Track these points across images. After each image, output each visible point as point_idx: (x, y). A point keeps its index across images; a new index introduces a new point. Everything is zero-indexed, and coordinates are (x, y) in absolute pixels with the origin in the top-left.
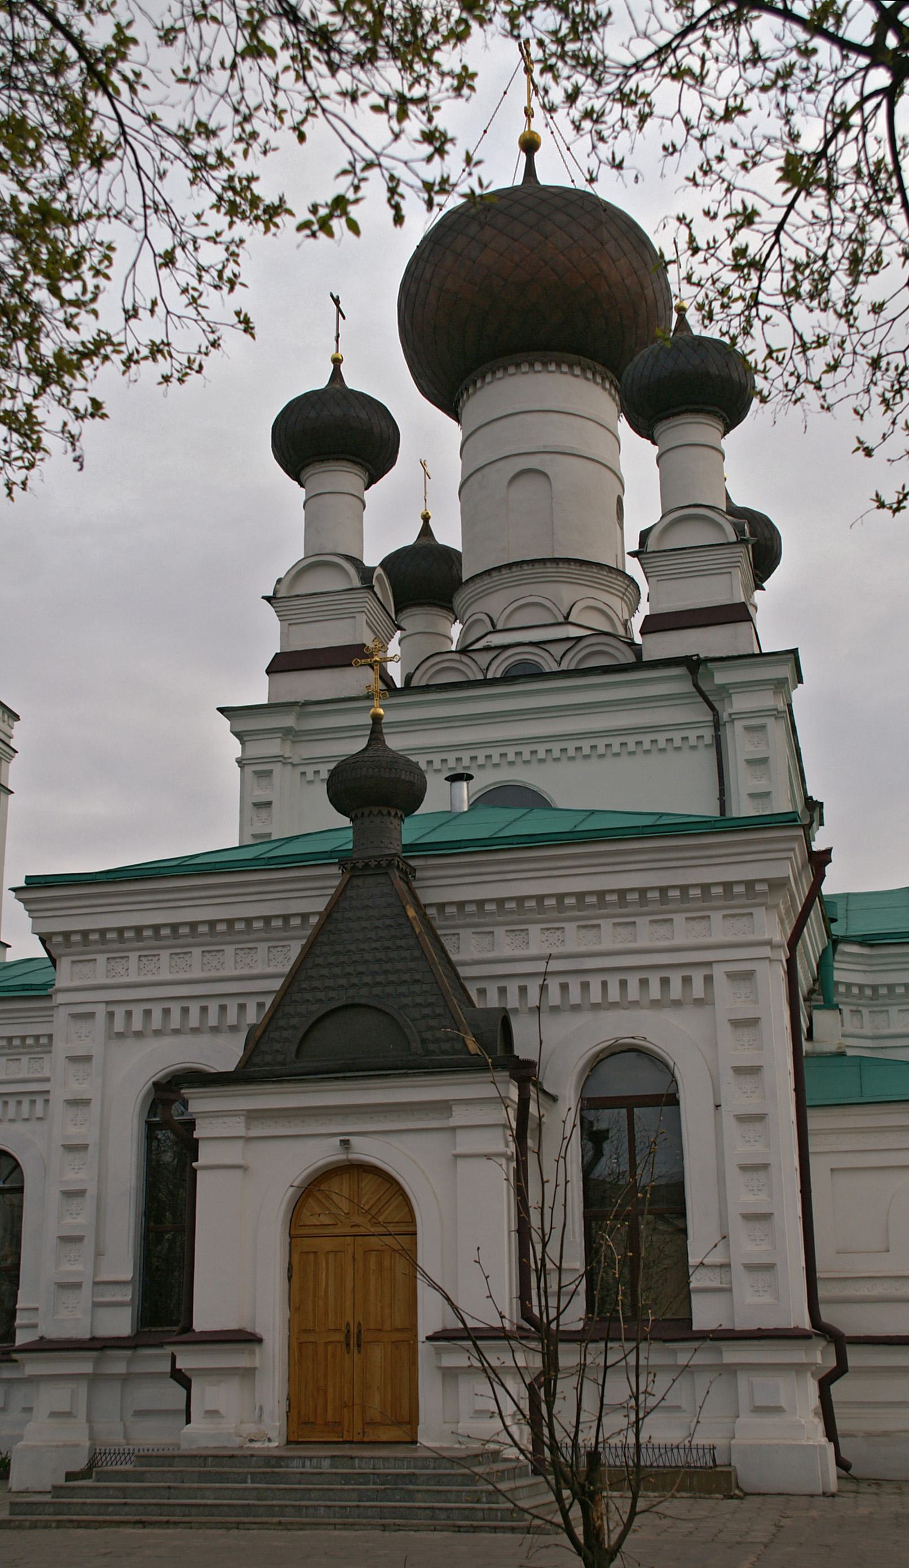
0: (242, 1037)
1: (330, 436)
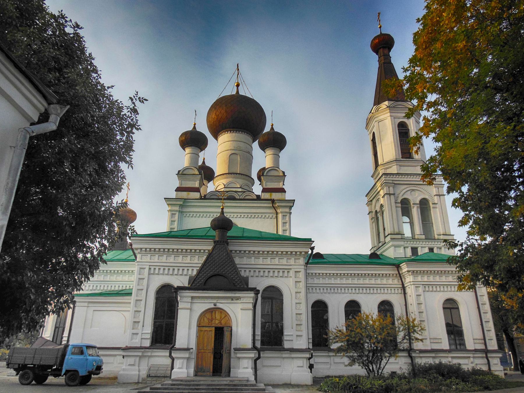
0: (188, 277)
1: (193, 140)
